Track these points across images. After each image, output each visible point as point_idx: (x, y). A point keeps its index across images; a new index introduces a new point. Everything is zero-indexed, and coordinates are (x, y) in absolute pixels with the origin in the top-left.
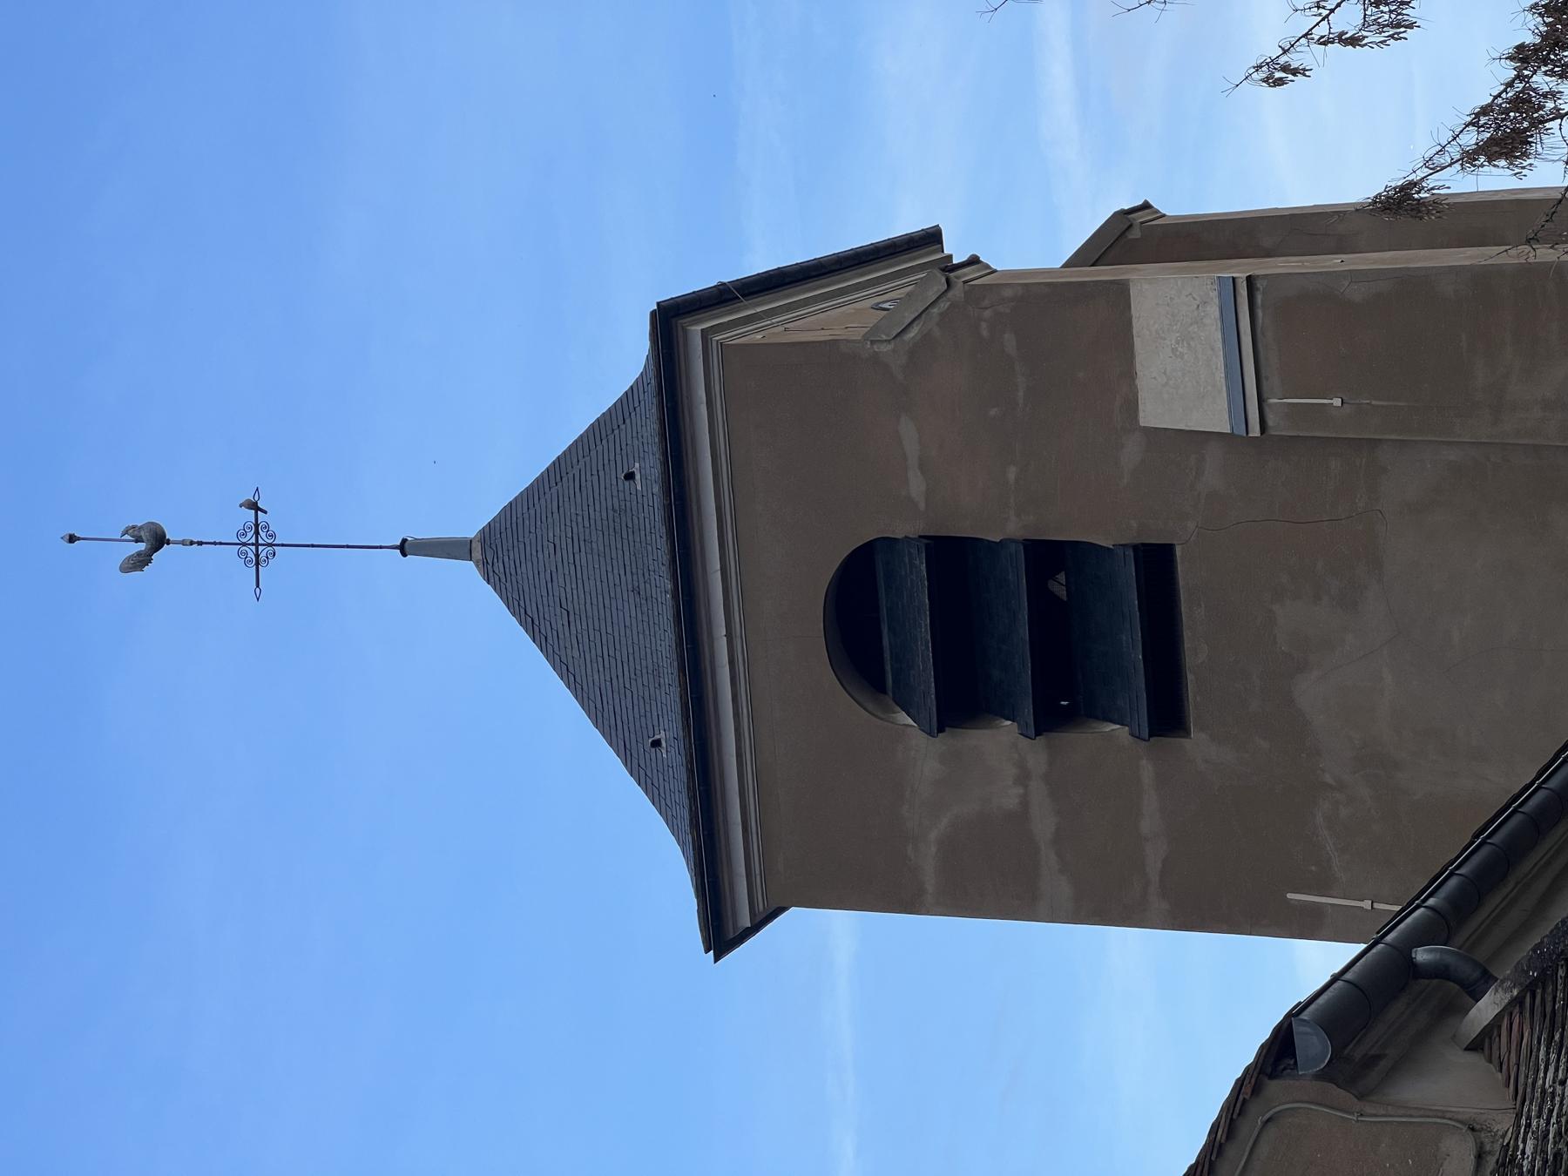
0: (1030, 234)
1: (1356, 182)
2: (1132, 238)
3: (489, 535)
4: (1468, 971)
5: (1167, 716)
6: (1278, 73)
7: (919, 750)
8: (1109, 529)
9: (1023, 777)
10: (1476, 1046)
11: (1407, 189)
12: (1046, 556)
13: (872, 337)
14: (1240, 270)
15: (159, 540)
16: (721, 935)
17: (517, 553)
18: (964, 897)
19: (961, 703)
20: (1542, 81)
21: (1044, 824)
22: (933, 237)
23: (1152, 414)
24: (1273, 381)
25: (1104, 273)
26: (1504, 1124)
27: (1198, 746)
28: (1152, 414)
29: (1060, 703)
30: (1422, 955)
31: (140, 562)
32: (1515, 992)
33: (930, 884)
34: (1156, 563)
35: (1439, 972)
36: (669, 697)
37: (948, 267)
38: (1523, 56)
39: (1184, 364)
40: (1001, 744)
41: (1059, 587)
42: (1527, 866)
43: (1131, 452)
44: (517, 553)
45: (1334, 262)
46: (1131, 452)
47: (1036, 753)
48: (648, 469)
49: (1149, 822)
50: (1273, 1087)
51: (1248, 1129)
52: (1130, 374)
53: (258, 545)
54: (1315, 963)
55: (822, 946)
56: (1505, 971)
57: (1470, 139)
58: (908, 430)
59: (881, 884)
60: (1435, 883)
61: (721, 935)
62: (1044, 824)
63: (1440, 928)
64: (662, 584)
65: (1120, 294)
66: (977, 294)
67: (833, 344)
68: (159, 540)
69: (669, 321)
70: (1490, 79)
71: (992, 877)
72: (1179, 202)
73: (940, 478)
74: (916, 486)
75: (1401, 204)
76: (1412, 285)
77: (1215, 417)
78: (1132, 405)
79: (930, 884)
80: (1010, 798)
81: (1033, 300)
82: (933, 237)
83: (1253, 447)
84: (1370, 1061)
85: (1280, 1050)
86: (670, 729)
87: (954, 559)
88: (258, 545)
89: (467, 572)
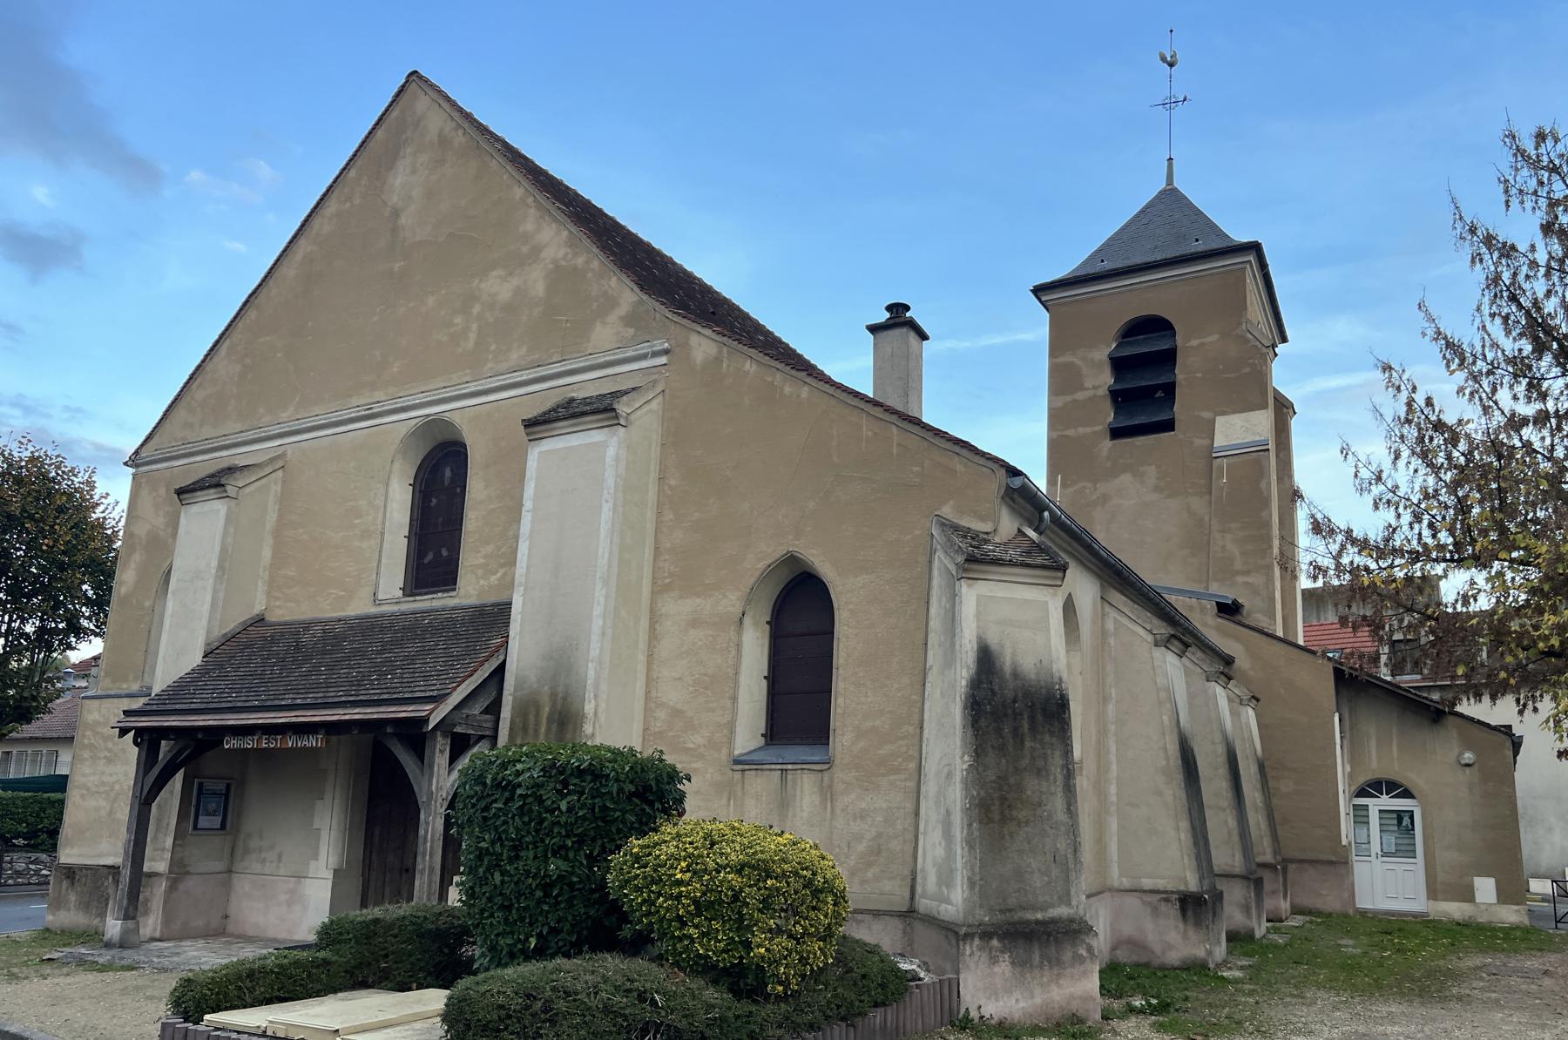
0: (1283, 376)
1: (195, 659)
2: (1283, 409)
3: (1176, 190)
4: (1042, 528)
5: (1117, 433)
6: (1345, 451)
7: (1103, 353)
8: (1181, 409)
9: (1095, 388)
10: (1019, 530)
11: (1301, 497)
12: (1170, 389)
13: (1248, 321)
14: (1272, 446)
15: (1171, 65)
16: (1038, 291)
17: (1170, 198)
18: (1055, 370)
19: (1119, 365)
20: (1340, 538)
21: (1080, 396)
22: (1284, 340)
23: (1220, 421)
24: (1231, 460)
25: (1271, 401)
26: (997, 540)
27: (1107, 444)
28: (1220, 421)
29: (1120, 398)
30: (1046, 514)
31: (1163, 59)
32: (195, 175)
33: (1061, 360)
34: (1169, 426)
35: (1041, 519)
36: (1120, 264)
37: (1274, 346)
38: (1349, 532)
39: (1237, 430)
40: (1106, 379)
41: (1159, 394)
42: (1075, 545)
43: (1207, 415)
44: (1170, 198)
45: (1274, 477)
46: (1207, 415)
47: (1103, 391)
48: (1201, 246)
49: (1081, 430)
50: (1003, 471)
51: (990, 464)
52: (1235, 412)
53: (1170, 103)
54: (1040, 481)
55: (1036, 327)
56: (1043, 538)
57: (1319, 516)
58: (1215, 337)
59: (1057, 345)
60: (1068, 517)
61: (1038, 291)
62: (1080, 396)
63: (1055, 519)
64: (1158, 256)
65: (1264, 406)
66: (1264, 357)
67: (1245, 308)
68: (1171, 65)
69: (1255, 248)
70: (1340, 522)
71: (1062, 379)
72: (1295, 424)
73: (1196, 352)
74: (1194, 343)
75: (1296, 495)
76: (1266, 502)
77: (1219, 441)
78: (1223, 413)
79: (1061, 360)
80: (1088, 384)
81: (1261, 378)
82: (1284, 340)
83: (1210, 455)
84: (1013, 500)
85: (1014, 472)
86: (1108, 265)
87: (1168, 358)
88: (1170, 103)
89: (1163, 185)
